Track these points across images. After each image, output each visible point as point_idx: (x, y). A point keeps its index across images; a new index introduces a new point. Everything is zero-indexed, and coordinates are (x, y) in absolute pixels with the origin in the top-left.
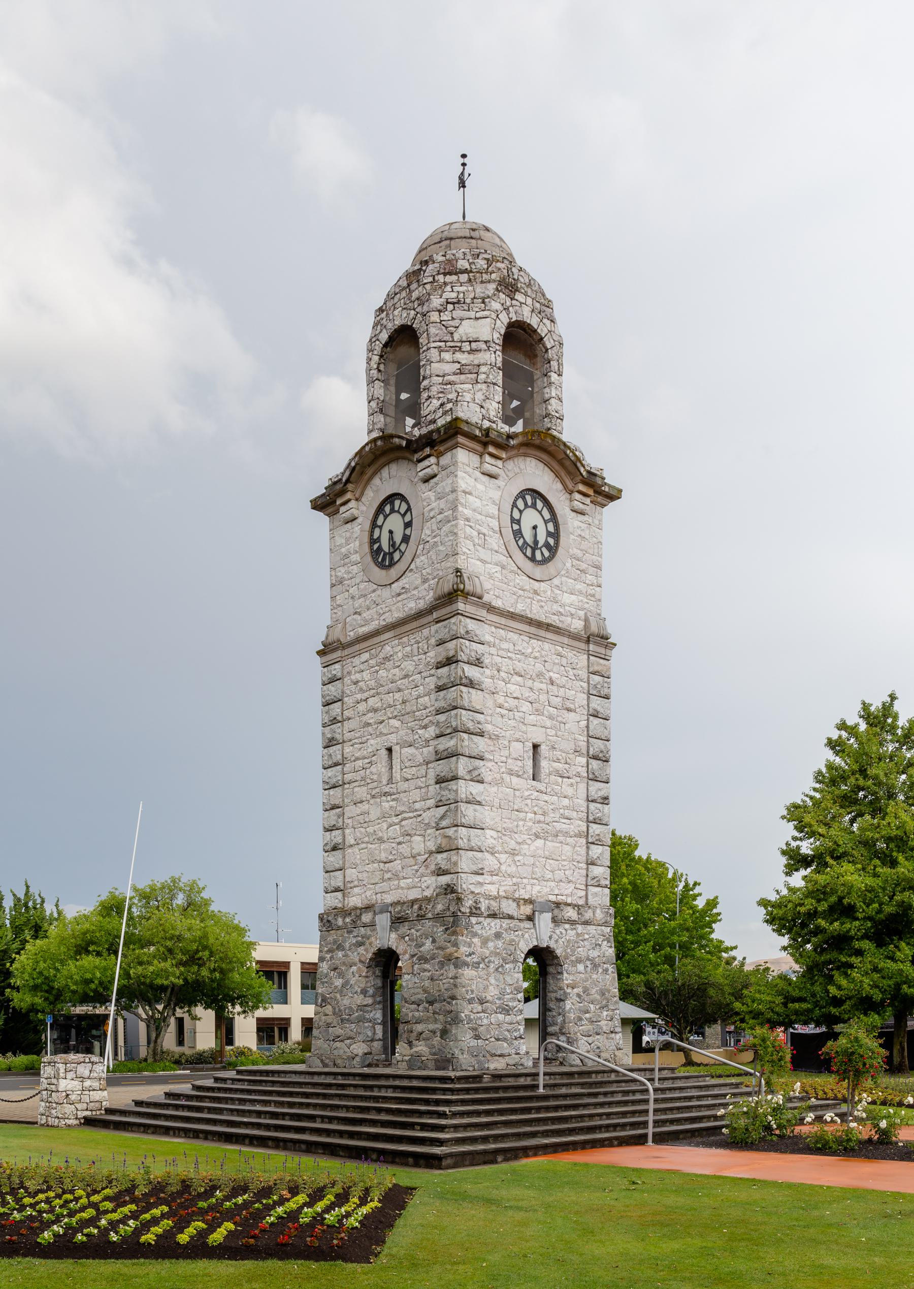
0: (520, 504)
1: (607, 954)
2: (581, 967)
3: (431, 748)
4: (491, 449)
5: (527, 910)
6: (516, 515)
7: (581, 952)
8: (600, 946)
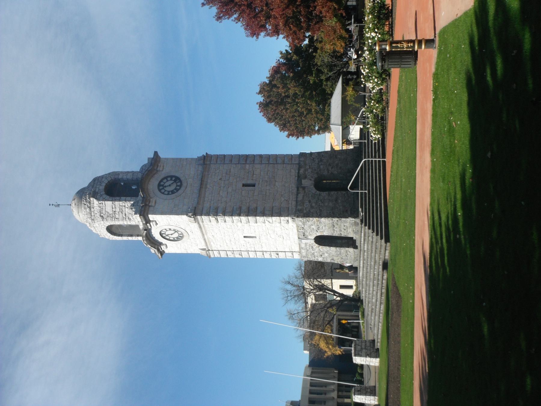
0: (163, 191)
2: (322, 167)
3: (245, 225)
5: (301, 189)
6: (166, 193)
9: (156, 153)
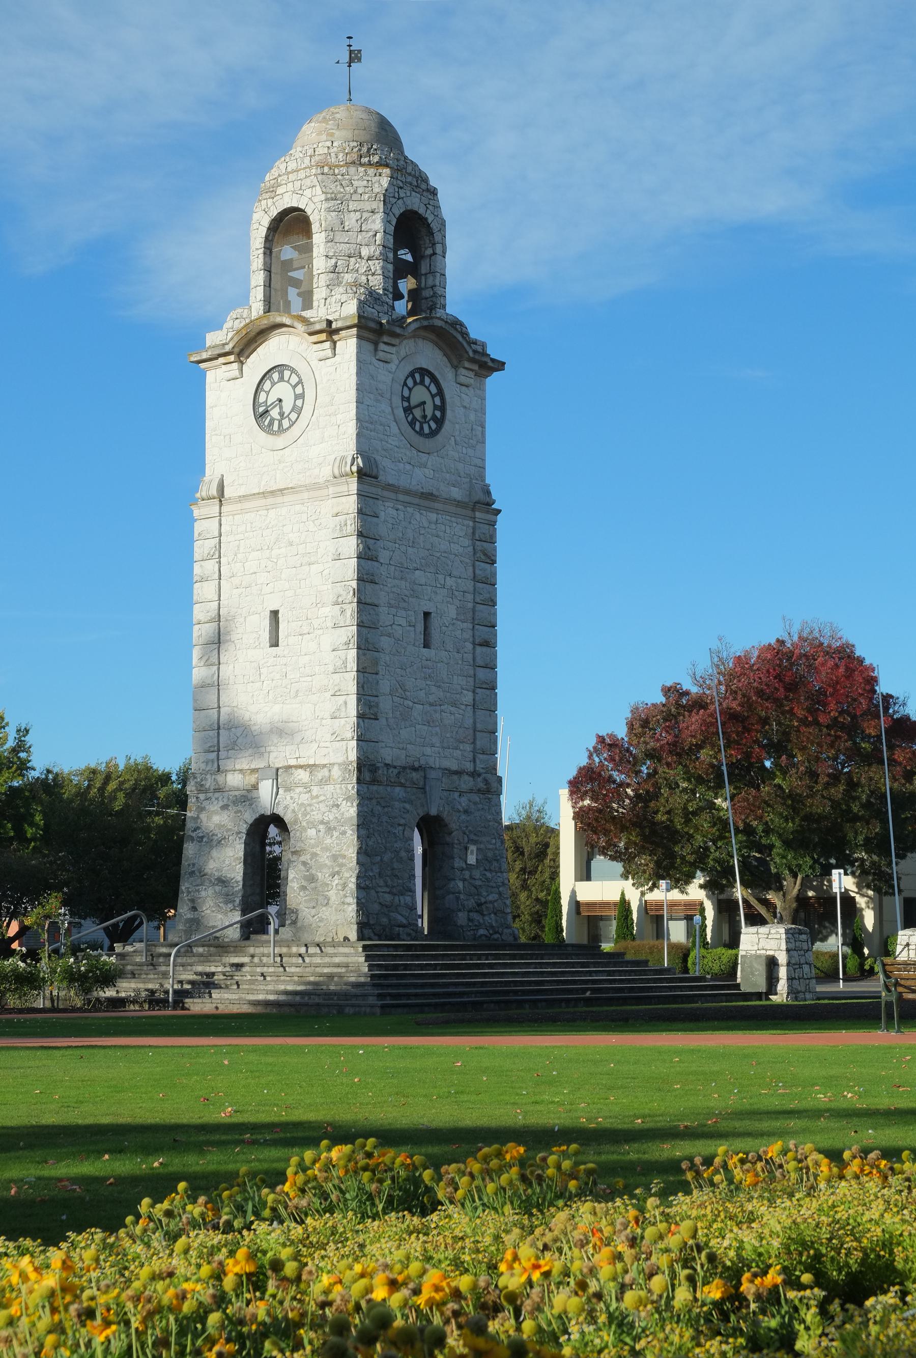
0: (410, 382)
1: (347, 815)
4: (386, 339)
7: (316, 816)
8: (338, 806)
9: (499, 366)
